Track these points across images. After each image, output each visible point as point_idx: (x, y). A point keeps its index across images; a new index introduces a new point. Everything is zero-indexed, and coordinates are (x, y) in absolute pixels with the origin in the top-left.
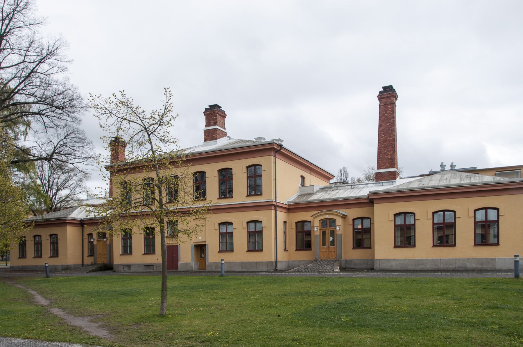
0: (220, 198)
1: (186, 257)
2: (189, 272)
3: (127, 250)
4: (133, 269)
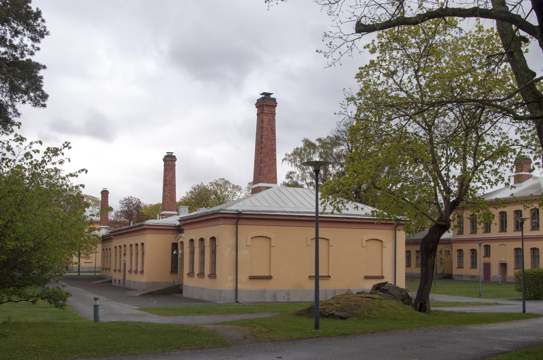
0: (500, 232)
1: (495, 272)
2: (496, 283)
3: (460, 266)
4: (464, 278)
